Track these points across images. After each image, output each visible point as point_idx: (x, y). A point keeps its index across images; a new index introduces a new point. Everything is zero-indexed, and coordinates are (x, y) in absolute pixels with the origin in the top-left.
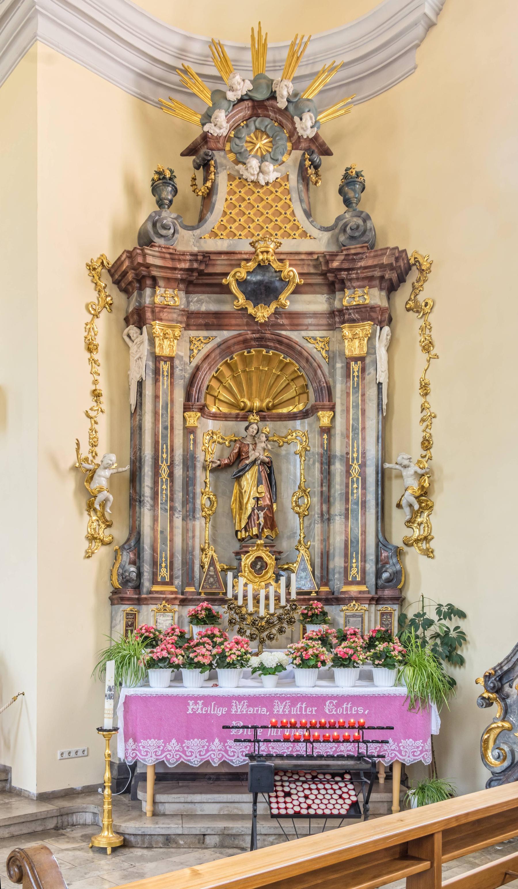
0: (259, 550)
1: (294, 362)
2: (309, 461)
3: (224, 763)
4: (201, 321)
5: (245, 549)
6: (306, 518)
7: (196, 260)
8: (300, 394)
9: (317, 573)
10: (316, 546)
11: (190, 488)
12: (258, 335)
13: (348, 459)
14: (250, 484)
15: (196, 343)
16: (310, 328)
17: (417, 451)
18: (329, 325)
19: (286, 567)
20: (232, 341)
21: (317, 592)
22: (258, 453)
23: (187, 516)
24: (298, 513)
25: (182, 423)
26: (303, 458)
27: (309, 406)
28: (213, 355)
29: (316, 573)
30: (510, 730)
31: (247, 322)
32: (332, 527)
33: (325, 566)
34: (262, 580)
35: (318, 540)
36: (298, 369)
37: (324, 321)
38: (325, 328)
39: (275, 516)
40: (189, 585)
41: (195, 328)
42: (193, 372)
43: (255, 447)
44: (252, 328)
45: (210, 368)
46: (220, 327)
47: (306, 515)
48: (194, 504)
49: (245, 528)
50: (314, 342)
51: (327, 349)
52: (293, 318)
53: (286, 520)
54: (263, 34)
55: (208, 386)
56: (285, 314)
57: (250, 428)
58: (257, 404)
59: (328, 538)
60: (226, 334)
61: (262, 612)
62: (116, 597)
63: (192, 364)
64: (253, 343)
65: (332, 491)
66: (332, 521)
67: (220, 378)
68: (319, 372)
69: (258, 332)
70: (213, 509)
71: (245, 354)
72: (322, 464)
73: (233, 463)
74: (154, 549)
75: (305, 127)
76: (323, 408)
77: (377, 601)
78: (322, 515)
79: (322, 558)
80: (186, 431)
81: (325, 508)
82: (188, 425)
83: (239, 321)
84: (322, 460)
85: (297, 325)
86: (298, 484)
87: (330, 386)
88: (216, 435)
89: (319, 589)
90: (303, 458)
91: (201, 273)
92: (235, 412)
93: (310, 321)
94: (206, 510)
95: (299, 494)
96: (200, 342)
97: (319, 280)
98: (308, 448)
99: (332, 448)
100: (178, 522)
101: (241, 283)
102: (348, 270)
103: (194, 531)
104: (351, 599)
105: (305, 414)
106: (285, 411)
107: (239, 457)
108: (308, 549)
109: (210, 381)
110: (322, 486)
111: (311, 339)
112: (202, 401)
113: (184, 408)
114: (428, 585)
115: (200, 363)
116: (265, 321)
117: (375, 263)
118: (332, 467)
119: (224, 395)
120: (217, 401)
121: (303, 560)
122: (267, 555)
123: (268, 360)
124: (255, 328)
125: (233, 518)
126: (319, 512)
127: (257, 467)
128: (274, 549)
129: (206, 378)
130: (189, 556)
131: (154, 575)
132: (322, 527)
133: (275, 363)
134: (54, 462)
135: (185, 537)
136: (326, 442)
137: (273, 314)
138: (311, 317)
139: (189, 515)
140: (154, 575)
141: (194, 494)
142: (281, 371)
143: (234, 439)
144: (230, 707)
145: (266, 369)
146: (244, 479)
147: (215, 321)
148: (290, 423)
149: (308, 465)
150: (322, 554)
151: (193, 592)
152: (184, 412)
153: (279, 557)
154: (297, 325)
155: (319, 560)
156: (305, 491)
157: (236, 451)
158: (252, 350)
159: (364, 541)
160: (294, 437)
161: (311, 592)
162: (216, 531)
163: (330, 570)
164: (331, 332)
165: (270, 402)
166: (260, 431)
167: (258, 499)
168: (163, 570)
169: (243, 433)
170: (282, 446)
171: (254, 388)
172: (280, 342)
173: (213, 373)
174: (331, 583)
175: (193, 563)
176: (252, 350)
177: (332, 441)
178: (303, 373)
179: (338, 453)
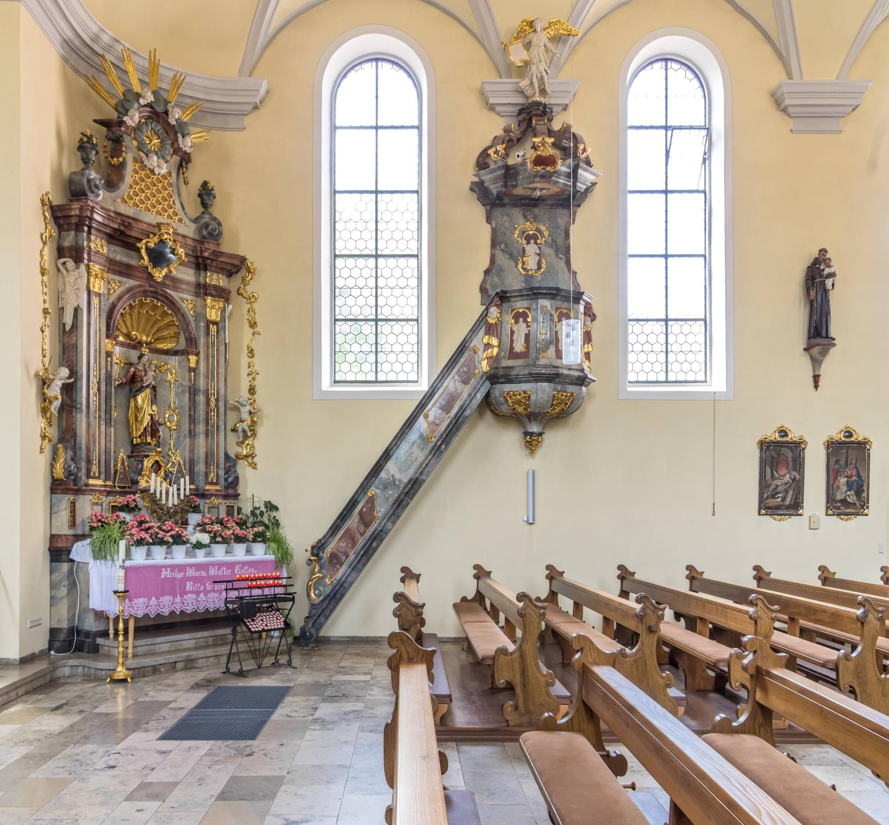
3: (182, 612)
7: (123, 225)
13: (208, 394)
17: (245, 394)
22: (149, 380)
30: (322, 578)
37: (193, 289)
46: (128, 276)
54: (157, 58)
61: (170, 505)
62: (56, 486)
74: (88, 450)
75: (186, 144)
76: (192, 354)
77: (226, 497)
83: (141, 275)
91: (122, 233)
93: (184, 287)
97: (193, 260)
100: (103, 427)
101: (148, 249)
102: (212, 260)
104: (212, 495)
111: (186, 300)
114: (254, 488)
117: (230, 262)
131: (89, 470)
133: (159, 311)
134: (27, 368)
140: (89, 470)
144: (185, 572)
159: (218, 454)
168: (94, 466)
172: (167, 298)
179: (202, 388)
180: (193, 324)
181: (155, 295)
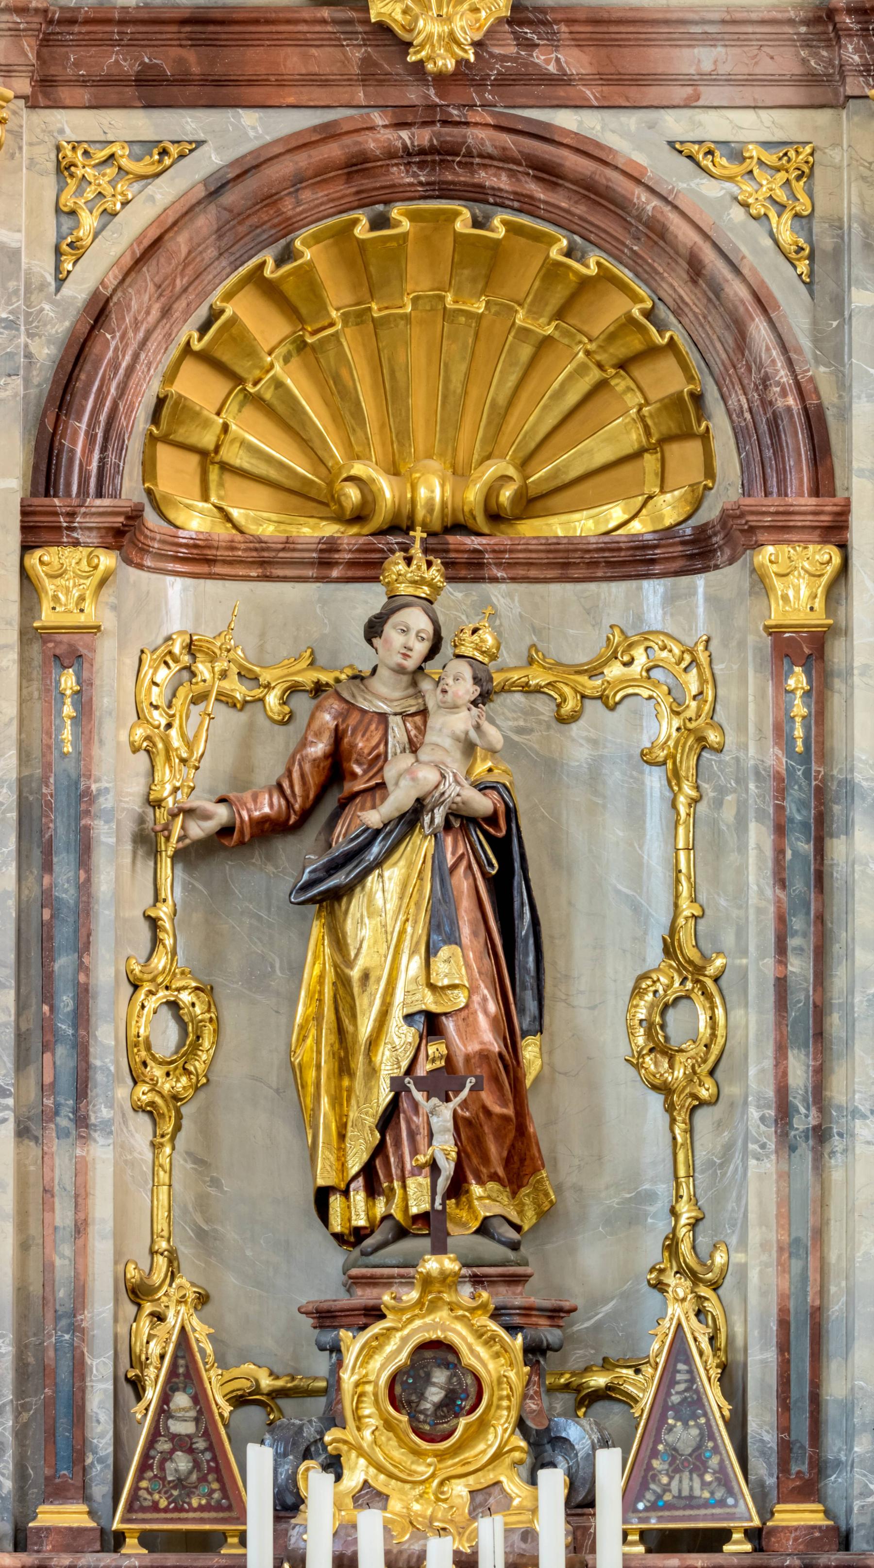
0: (433, 1306)
1: (625, 275)
2: (718, 803)
4: (118, 61)
5: (364, 1296)
6: (703, 1118)
8: (664, 440)
9: (762, 1425)
10: (754, 1276)
11: (63, 963)
12: (424, 137)
14: (395, 935)
15: (90, 172)
16: (709, 95)
18: (811, 79)
19: (599, 1380)
20: (285, 168)
21: (754, 1535)
23: (48, 1116)
24: (664, 1089)
25: (14, 610)
26: (688, 790)
27: (709, 513)
28: (181, 242)
29: (753, 1425)
31: (366, 61)
32: (837, 1175)
33: (800, 1391)
34: (451, 1466)
35: (764, 1246)
36: (649, 314)
37: (784, 61)
38: (789, 94)
39: (535, 1109)
40: (57, 1492)
41: (85, 95)
42: (73, 333)
43: (422, 731)
44: (394, 96)
45: (166, 312)
46: (219, 91)
47: (702, 1103)
48: (82, 1049)
49: (369, 1172)
50: (735, 169)
51: (803, 206)
52: (617, 43)
53: (596, 1120)
55: (160, 402)
56: (570, 22)
57: (390, 630)
58: (432, 491)
59: (819, 1234)
60: (252, 128)
63: (67, 290)
64: (400, 175)
65: (839, 980)
66: (837, 1143)
67: (226, 356)
68: (760, 331)
69: (430, 116)
70: (198, 1066)
71: (362, 231)
72: (780, 830)
73: (306, 815)
76: (783, 529)
78: (784, 1111)
79: (784, 1347)
80: (36, 648)
81: (799, 1073)
82: (47, 617)
83: (322, 59)
84: (780, 809)
85: (640, 80)
86: (661, 918)
87: (820, 408)
88: (213, 658)
89: (766, 1513)
90: (688, 790)
92: (313, 530)
93: (704, 58)
94: (158, 1072)
95: (669, 982)
96: (111, 171)
98: (713, 737)
99: (837, 743)
103: (81, 1198)
105: (696, 550)
106: (581, 525)
107: (336, 777)
108: (715, 1286)
109: (170, 376)
110: (781, 949)
112: (131, 489)
113: (26, 529)
115: (112, 281)
116: (461, 63)
118: (837, 848)
119: (253, 438)
120: (214, 474)
121: (679, 1348)
122: (479, 1334)
123: (484, 262)
124: (413, 95)
125: (305, 1119)
126: (770, 1093)
127: (428, 846)
128: (516, 1297)
129: (147, 366)
130: (56, 1336)
132: (785, 1176)
133: (524, 278)
135: (34, 1229)
136: (799, 709)
137: (500, 21)
138: (709, 40)
139: (57, 1106)
141: (83, 995)
142: (560, 315)
143: (308, 678)
145: (479, 307)
146: (357, 905)
147: (193, 60)
148: (615, 593)
149: (714, 824)
150: (784, 1324)
151: (80, 1531)
152: (26, 548)
153: (550, 1335)
154: (640, 80)
155: (772, 1355)
156: (694, 971)
157: (319, 748)
158: (396, 212)
160: (637, 669)
161: (725, 1535)
162: (215, 1183)
163: (831, 1413)
164: (823, 117)
165: (505, 479)
166: (447, 649)
167: (432, 1025)
169: (362, 657)
170: (574, 717)
171: (419, 401)
172: (548, 173)
173: (188, 332)
174: (834, 1481)
175: (79, 1370)
176: (396, 212)
177: (836, 702)
178: (676, 332)
180: (796, 312)
181: (444, 169)
